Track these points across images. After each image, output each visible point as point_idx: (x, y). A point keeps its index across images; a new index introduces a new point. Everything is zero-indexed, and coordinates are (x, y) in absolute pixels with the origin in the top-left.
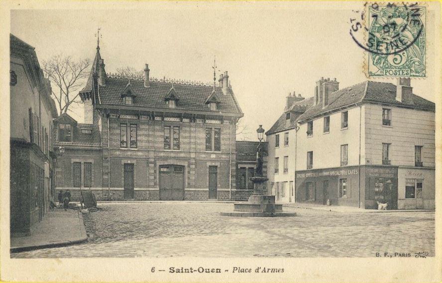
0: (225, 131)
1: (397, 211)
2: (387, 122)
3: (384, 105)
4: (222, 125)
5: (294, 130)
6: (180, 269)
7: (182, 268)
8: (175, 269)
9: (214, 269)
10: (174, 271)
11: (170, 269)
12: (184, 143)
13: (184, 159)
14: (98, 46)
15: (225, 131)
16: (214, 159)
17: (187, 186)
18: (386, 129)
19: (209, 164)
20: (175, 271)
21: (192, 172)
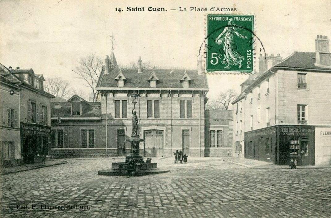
0: (195, 103)
1: (305, 89)
2: (301, 85)
3: (299, 70)
4: (193, 98)
5: (244, 99)
6: (135, 8)
7: (136, 7)
8: (131, 8)
9: (159, 9)
10: (130, 10)
11: (128, 8)
12: (163, 113)
13: (163, 125)
14: (113, 48)
15: (195, 103)
16: (186, 125)
17: (165, 146)
18: (302, 92)
19: (183, 128)
20: (132, 9)
21: (169, 135)
